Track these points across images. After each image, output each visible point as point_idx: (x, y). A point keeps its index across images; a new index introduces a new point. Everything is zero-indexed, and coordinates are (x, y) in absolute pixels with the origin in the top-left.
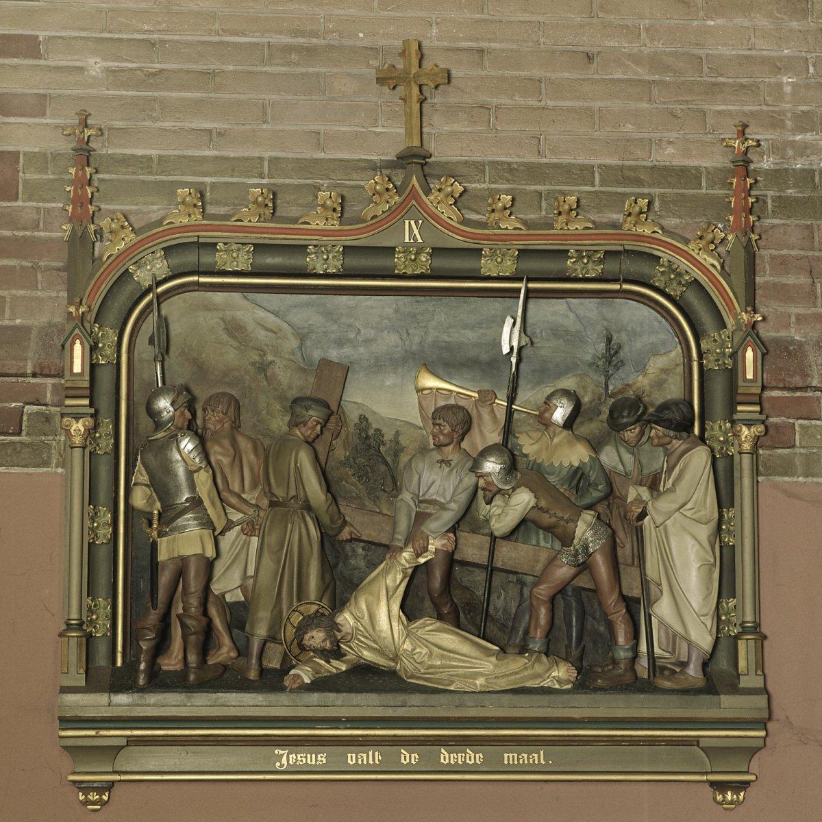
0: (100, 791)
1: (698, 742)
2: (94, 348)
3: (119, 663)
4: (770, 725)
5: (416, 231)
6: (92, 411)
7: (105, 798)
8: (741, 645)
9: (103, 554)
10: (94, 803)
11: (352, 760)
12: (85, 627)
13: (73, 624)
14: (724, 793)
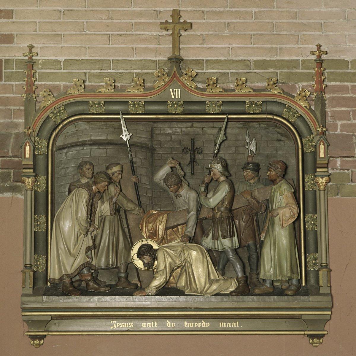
1: (301, 316)
2: (34, 149)
4: (333, 310)
6: (34, 174)
7: (42, 342)
8: (321, 273)
10: (316, 343)
11: (169, 325)
12: (33, 268)
13: (29, 266)
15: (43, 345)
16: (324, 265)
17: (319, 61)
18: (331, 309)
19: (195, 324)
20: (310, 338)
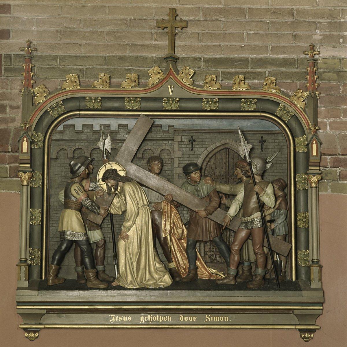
0: (35, 332)
1: (293, 311)
2: (32, 142)
4: (324, 305)
6: (31, 170)
7: (37, 335)
10: (32, 338)
11: (191, 319)
12: (28, 262)
13: (24, 260)
14: (29, 332)
15: (38, 338)
18: (321, 304)
19: (165, 317)
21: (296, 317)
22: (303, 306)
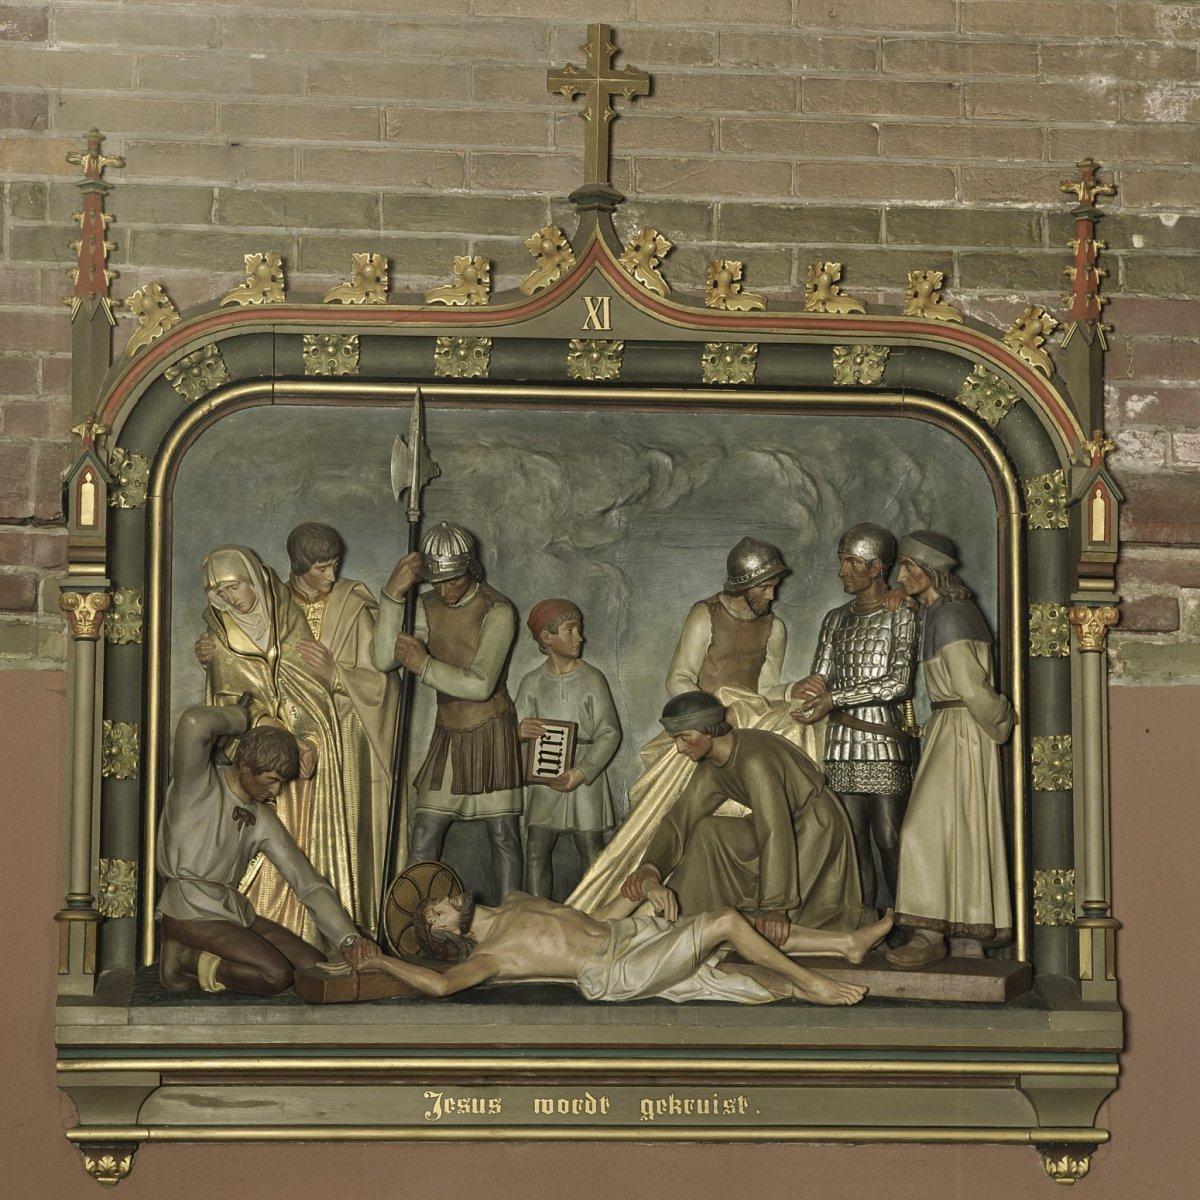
1: (1018, 1080)
2: (113, 487)
3: (149, 961)
4: (1126, 1059)
5: (593, 313)
6: (107, 583)
7: (125, 1165)
8: (1084, 936)
9: (124, 797)
11: (591, 1109)
12: (95, 905)
13: (1096, 909)
14: (97, 1157)
16: (79, 898)
17: (91, 190)
18: (1117, 1055)
19: (658, 1102)
20: (1044, 1154)
21: (1031, 1100)
22: (969, 1062)
